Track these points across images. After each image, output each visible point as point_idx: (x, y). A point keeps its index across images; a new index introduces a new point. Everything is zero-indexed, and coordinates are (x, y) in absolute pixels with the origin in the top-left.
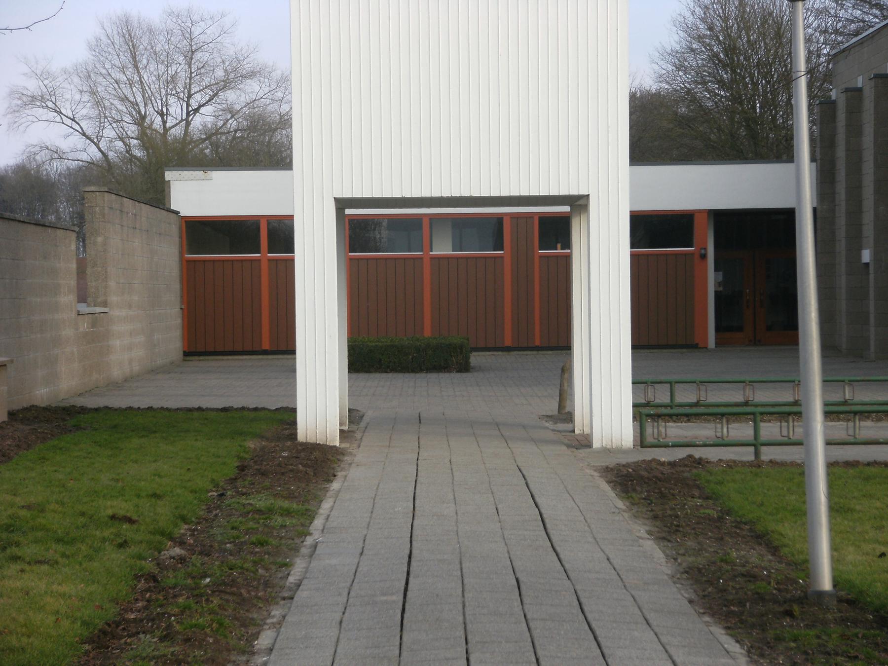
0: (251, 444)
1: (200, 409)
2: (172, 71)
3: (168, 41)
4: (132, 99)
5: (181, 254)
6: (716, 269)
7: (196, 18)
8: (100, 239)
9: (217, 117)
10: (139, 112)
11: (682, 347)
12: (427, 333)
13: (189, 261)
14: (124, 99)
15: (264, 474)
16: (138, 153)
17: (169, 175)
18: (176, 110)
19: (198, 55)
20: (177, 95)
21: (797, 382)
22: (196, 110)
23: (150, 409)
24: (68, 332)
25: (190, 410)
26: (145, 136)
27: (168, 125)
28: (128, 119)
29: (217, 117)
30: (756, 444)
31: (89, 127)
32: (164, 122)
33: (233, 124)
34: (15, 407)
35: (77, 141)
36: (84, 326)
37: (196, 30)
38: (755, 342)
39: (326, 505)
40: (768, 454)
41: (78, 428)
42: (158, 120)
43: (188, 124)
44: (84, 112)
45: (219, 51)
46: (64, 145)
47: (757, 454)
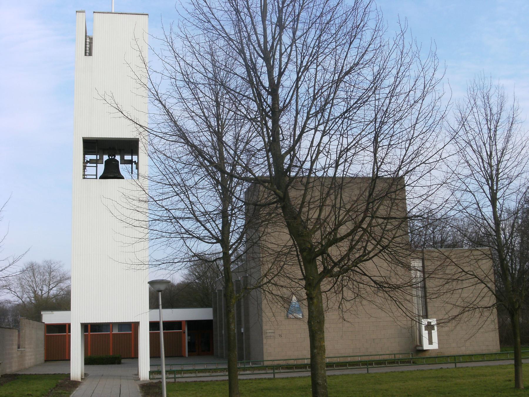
0: (60, 381)
1: (48, 374)
2: (44, 278)
3: (44, 269)
4: (32, 286)
5: (45, 334)
6: (188, 335)
7: (52, 262)
8: (24, 331)
9: (57, 291)
10: (34, 290)
11: (129, 358)
12: (111, 354)
13: (47, 336)
14: (30, 286)
15: (62, 387)
16: (33, 302)
17: (42, 313)
18: (45, 289)
19: (52, 273)
20: (46, 285)
21: (160, 365)
22: (51, 289)
23: (36, 374)
24: (15, 355)
25: (46, 374)
26: (36, 296)
27: (43, 293)
28: (31, 292)
29: (57, 291)
30: (175, 378)
31: (19, 294)
32: (42, 293)
33: (62, 293)
34: (2, 374)
35: (16, 298)
36: (19, 354)
37: (52, 266)
38: (199, 355)
39: (74, 392)
40: (177, 380)
41: (18, 378)
42: (40, 292)
43: (49, 293)
44: (18, 290)
45: (59, 272)
46: (12, 299)
47: (175, 380)
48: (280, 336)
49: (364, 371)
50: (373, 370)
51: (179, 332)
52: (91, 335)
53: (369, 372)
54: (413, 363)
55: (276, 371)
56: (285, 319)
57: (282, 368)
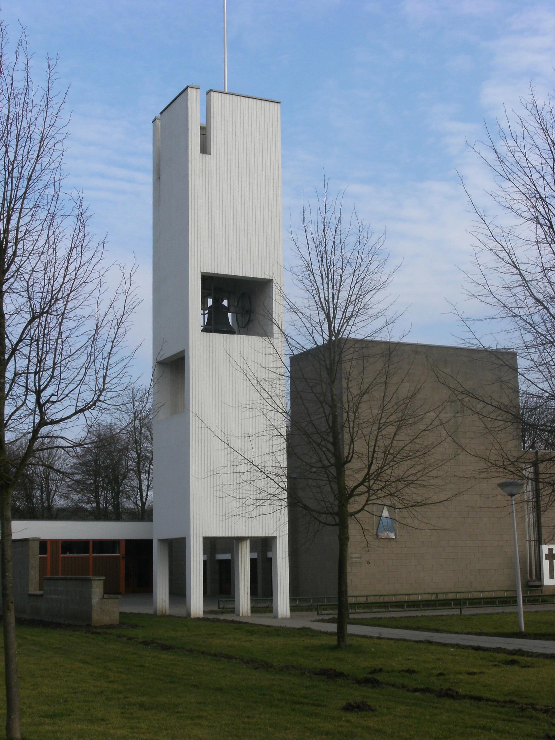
48: (368, 562)
49: (456, 612)
50: (467, 612)
51: (85, 557)
52: (94, 557)
53: (463, 613)
54: (542, 601)
55: (462, 607)
56: (374, 539)
57: (358, 607)
